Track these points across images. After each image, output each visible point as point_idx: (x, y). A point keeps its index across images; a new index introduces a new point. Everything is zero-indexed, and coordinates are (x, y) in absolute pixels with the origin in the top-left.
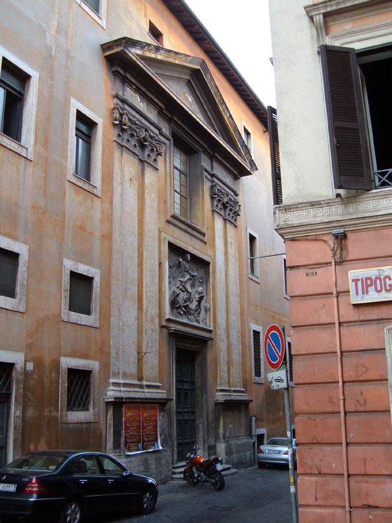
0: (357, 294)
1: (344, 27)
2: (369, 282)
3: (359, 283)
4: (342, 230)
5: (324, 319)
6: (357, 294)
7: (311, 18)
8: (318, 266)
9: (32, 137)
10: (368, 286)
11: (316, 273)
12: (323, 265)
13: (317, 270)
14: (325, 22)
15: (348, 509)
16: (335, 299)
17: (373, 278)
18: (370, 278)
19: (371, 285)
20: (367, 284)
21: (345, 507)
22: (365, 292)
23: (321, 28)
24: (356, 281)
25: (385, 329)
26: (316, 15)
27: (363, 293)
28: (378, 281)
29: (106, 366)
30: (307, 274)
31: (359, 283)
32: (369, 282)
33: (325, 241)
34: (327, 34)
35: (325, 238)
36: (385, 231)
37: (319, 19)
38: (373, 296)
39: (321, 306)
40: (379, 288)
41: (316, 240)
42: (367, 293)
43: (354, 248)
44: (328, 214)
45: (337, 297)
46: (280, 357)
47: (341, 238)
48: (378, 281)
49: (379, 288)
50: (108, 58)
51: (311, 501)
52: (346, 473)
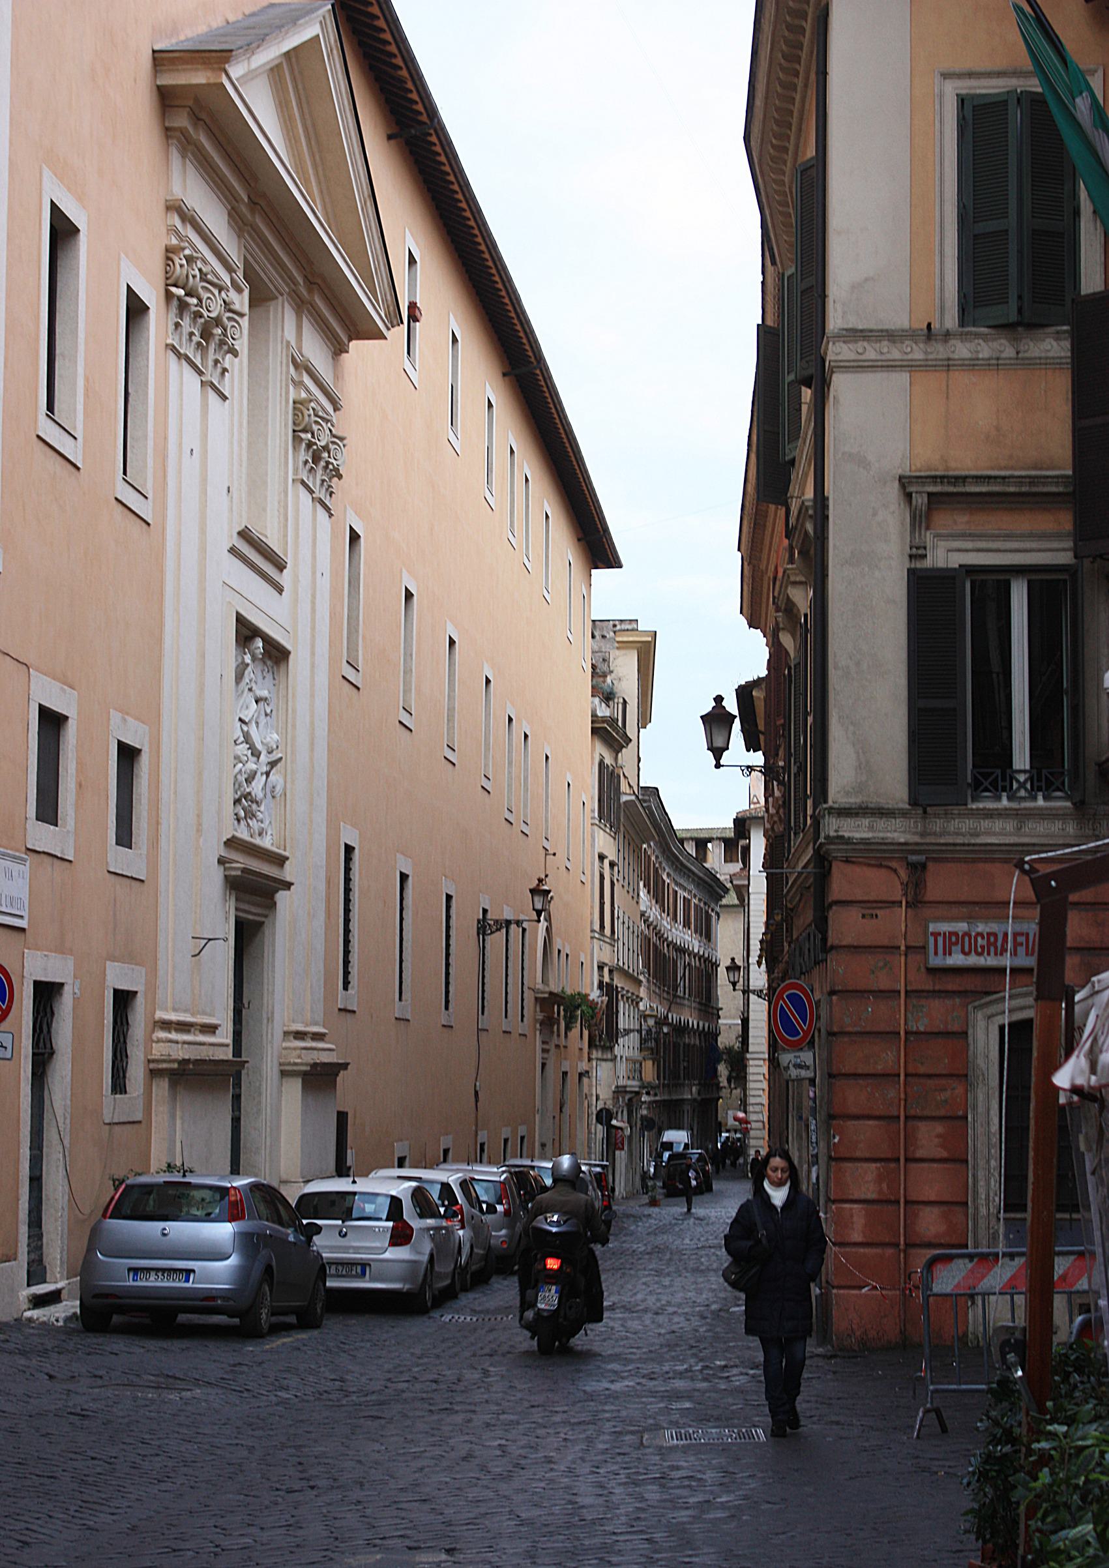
0: (936, 953)
1: (955, 517)
2: (954, 939)
3: (940, 940)
4: (922, 858)
5: (884, 983)
6: (936, 953)
7: (909, 496)
8: (880, 905)
9: (145, 814)
10: (951, 944)
11: (876, 916)
12: (887, 905)
13: (878, 912)
14: (929, 509)
15: (902, 1247)
16: (903, 958)
17: (960, 934)
18: (956, 934)
19: (956, 943)
20: (952, 941)
21: (898, 1245)
22: (948, 952)
23: (921, 516)
24: (936, 935)
25: (970, 1007)
26: (917, 492)
27: (945, 954)
28: (967, 939)
29: (152, 987)
30: (864, 916)
31: (940, 940)
32: (954, 939)
33: (895, 871)
34: (928, 528)
35: (894, 864)
36: (981, 865)
37: (920, 501)
38: (957, 959)
39: (881, 964)
40: (967, 949)
41: (881, 866)
42: (950, 954)
43: (939, 884)
44: (902, 829)
45: (906, 955)
46: (780, 997)
47: (917, 869)
48: (967, 939)
49: (967, 949)
50: (166, 98)
51: (233, 76)
52: (902, 1200)
